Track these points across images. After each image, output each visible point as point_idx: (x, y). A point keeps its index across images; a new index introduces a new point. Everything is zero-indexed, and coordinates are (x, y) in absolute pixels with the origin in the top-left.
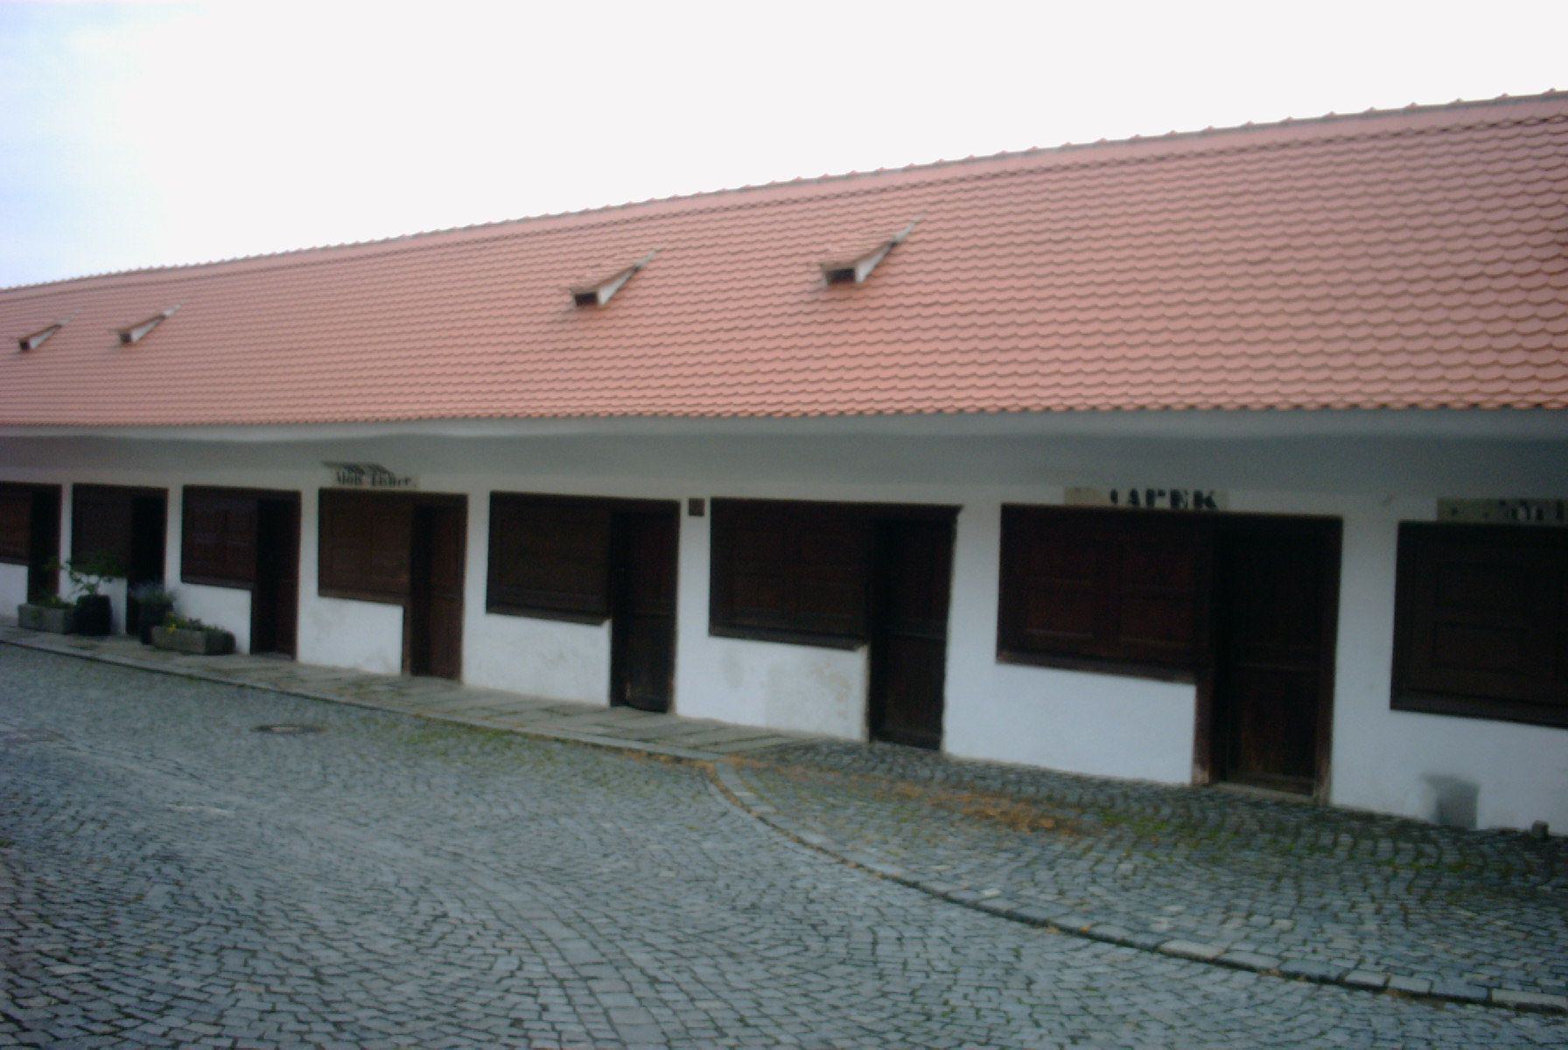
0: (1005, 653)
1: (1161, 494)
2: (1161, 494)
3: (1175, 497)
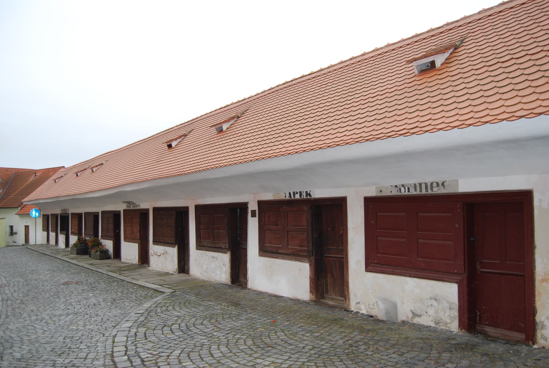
2: (297, 193)
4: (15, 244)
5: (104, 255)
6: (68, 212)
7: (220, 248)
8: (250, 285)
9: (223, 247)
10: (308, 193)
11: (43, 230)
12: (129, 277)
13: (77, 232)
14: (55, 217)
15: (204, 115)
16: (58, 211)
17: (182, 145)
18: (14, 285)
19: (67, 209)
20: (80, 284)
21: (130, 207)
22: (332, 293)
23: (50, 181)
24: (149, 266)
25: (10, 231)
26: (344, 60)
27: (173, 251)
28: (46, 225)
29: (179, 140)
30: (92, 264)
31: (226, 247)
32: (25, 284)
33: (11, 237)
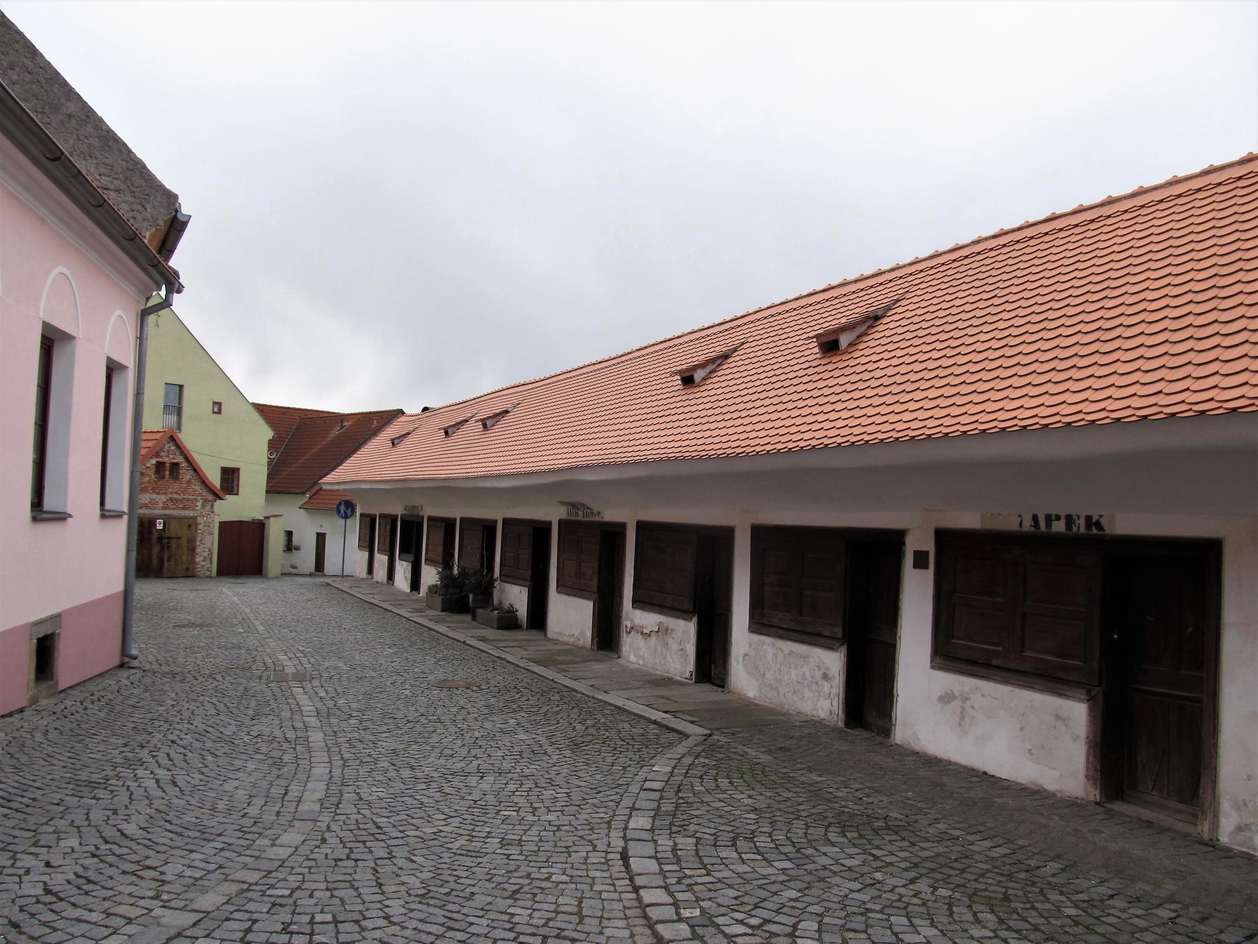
0: (938, 660)
1: (1058, 518)
2: (1058, 518)
3: (1070, 520)
4: (294, 571)
5: (508, 622)
6: (421, 514)
7: (820, 635)
8: (900, 735)
9: (826, 633)
10: (1094, 520)
11: (360, 547)
12: (582, 681)
13: (440, 559)
14: (389, 521)
15: (780, 304)
16: (398, 510)
17: (722, 379)
18: (331, 678)
19: (418, 507)
20: (475, 688)
21: (577, 514)
22: (1150, 787)
23: (380, 442)
24: (619, 657)
25: (286, 543)
26: (1181, 174)
27: (685, 631)
28: (367, 539)
29: (711, 367)
30: (483, 639)
31: (836, 634)
32: (354, 678)
33: (287, 555)
